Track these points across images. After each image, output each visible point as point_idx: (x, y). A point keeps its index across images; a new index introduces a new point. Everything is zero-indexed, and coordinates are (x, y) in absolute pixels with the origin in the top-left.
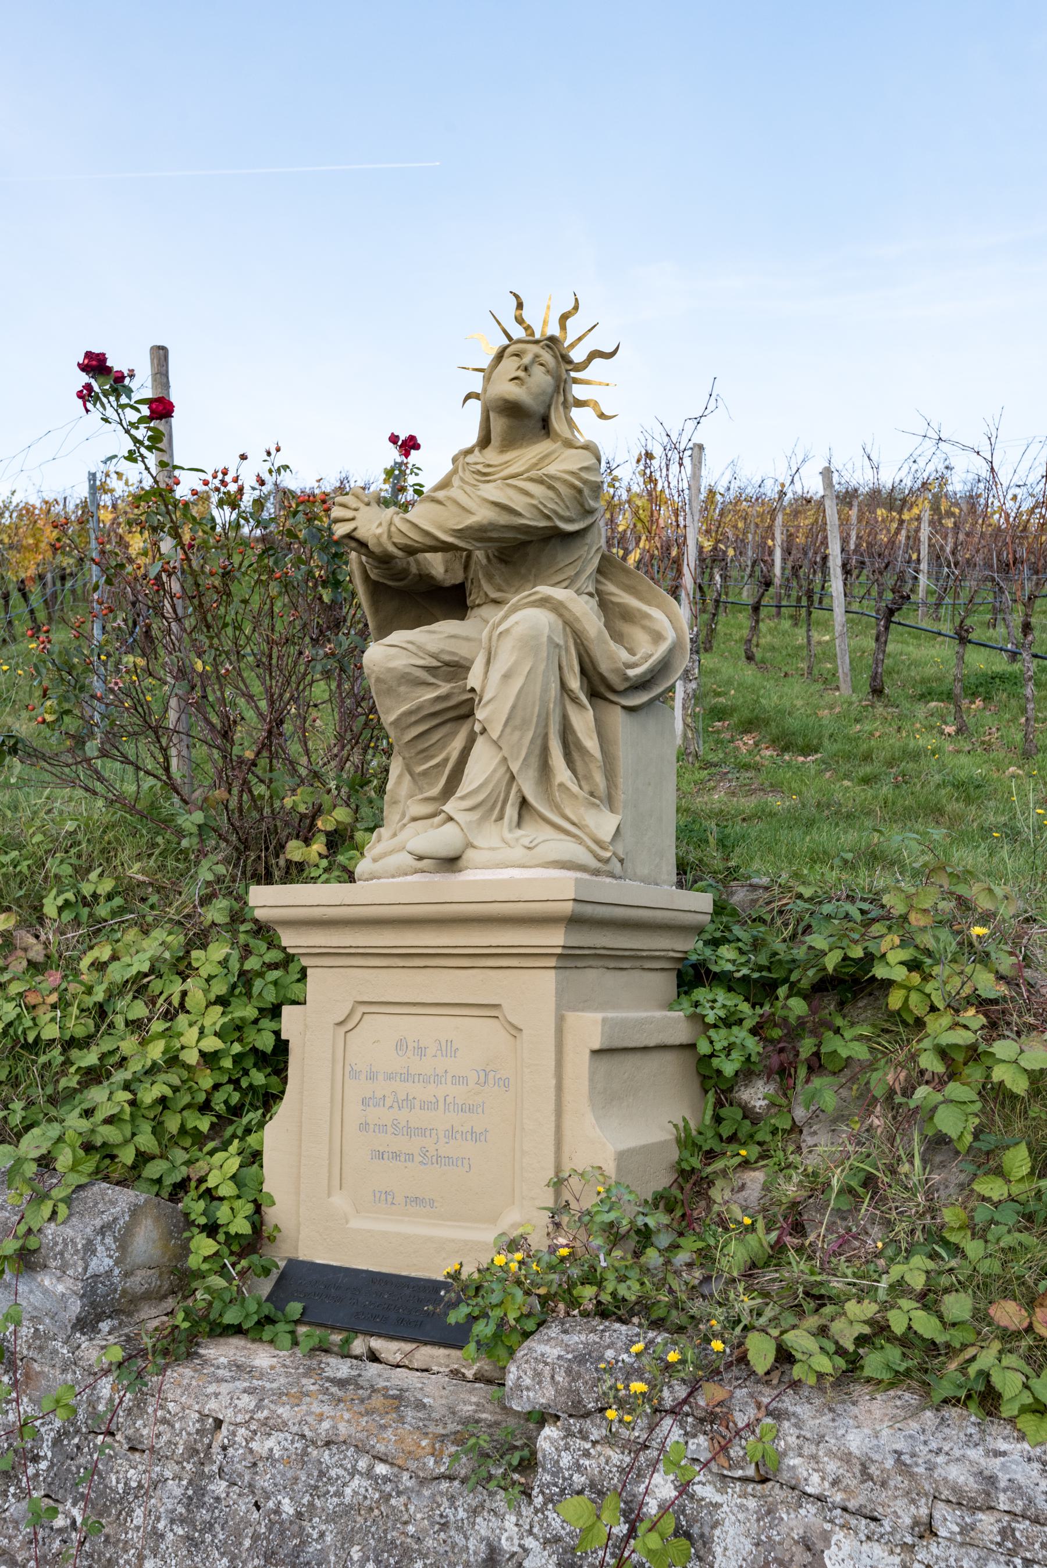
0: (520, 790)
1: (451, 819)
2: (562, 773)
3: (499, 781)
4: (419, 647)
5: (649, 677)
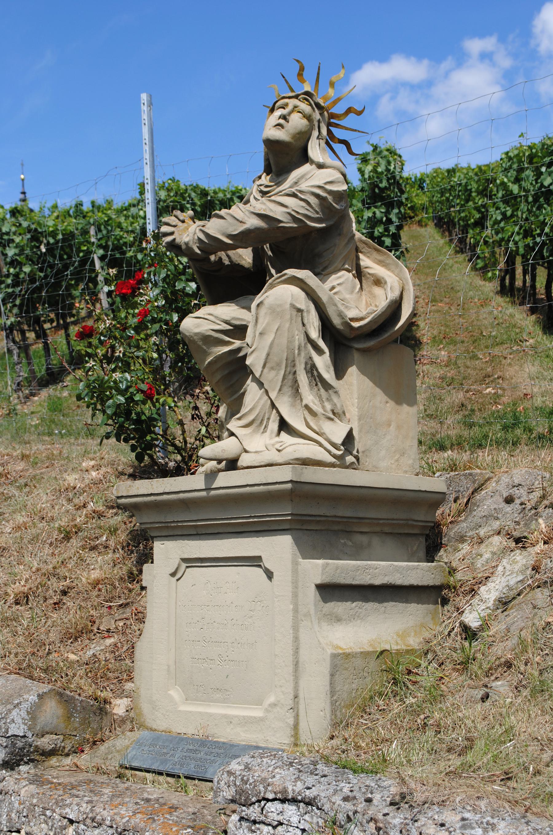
0: (278, 412)
1: (232, 434)
3: (264, 405)
4: (216, 317)
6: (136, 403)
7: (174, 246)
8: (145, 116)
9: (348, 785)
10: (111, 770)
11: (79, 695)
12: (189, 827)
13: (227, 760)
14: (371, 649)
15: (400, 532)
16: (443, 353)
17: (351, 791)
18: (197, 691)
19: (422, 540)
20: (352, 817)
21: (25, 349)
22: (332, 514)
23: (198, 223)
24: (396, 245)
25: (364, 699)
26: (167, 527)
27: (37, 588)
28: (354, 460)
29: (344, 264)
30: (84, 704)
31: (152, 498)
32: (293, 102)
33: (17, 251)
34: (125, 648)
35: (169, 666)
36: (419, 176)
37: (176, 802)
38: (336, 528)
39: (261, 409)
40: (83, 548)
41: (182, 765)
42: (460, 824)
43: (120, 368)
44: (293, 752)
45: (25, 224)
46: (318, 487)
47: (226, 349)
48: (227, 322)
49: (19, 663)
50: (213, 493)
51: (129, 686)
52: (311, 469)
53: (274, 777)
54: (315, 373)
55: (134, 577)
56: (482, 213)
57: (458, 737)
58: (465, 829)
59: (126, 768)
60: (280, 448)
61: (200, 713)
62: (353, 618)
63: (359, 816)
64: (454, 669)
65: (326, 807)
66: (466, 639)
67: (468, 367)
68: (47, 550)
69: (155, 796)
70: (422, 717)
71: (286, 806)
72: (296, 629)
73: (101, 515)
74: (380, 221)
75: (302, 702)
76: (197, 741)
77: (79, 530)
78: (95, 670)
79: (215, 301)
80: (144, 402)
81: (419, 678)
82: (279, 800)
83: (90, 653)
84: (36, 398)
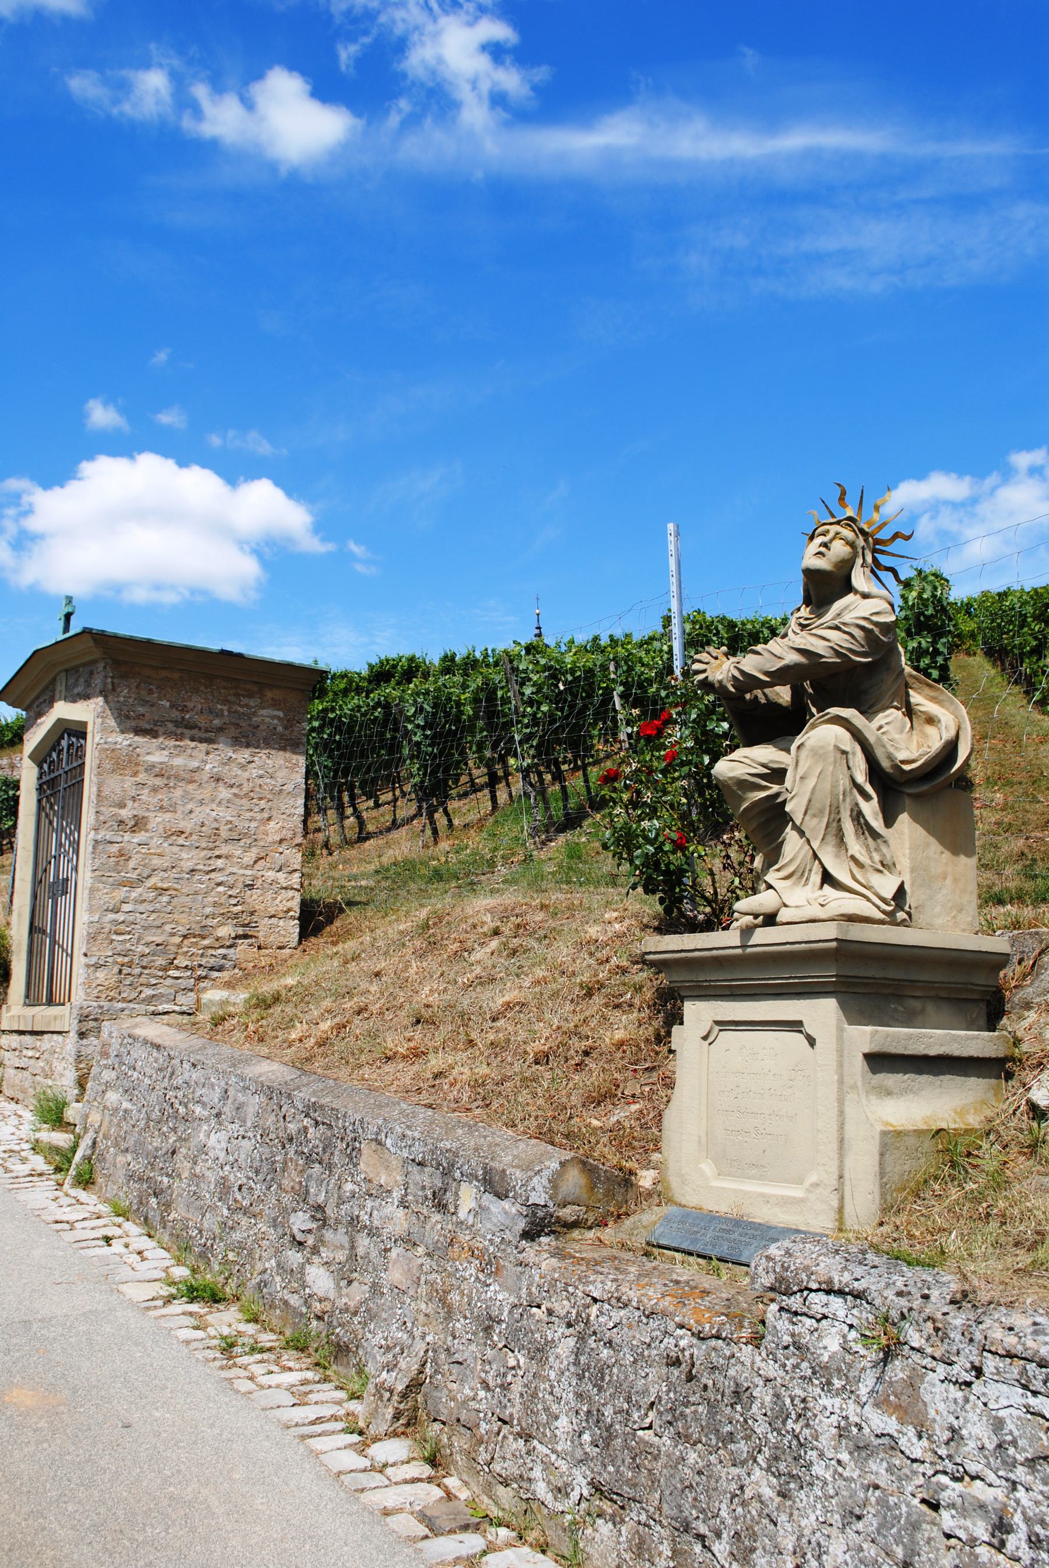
0: (821, 863)
1: (770, 887)
3: (805, 856)
4: (752, 760)
6: (666, 853)
7: (707, 685)
8: (672, 547)
9: (901, 1279)
10: (637, 1248)
11: (603, 1164)
12: (723, 1314)
13: (764, 1243)
14: (925, 1127)
15: (957, 996)
16: (998, 795)
17: (906, 1285)
18: (732, 1165)
19: (983, 1006)
20: (907, 1315)
21: (542, 793)
22: (881, 976)
23: (732, 659)
24: (944, 678)
25: (918, 1182)
26: (700, 987)
27: (558, 1048)
28: (905, 916)
29: (892, 702)
30: (608, 1175)
31: (683, 955)
32: (834, 529)
33: (534, 690)
34: (651, 1115)
35: (700, 1137)
36: (965, 600)
37: (707, 1286)
38: (886, 991)
39: (802, 859)
40: (606, 1005)
41: (714, 1246)
42: (1032, 1329)
43: (648, 814)
44: (838, 1238)
45: (543, 662)
46: (867, 946)
47: (763, 794)
49: (539, 1127)
50: (749, 950)
51: (655, 1156)
53: (818, 1265)
54: (862, 821)
55: (662, 1038)
56: (1039, 640)
57: (1026, 1230)
58: (1037, 1335)
59: (653, 1246)
61: (734, 1190)
62: (905, 1091)
63: (914, 1314)
64: (1020, 1152)
65: (878, 1302)
66: (1033, 1119)
67: (1027, 811)
68: (568, 1007)
69: (685, 1278)
70: (984, 1205)
71: (832, 1297)
72: (841, 1101)
73: (624, 971)
74: (926, 652)
75: (847, 1183)
76: (731, 1220)
77: (602, 986)
78: (619, 1138)
79: (750, 743)
80: (674, 852)
81: (980, 1162)
82: (824, 1290)
83: (613, 1119)
84: (553, 844)
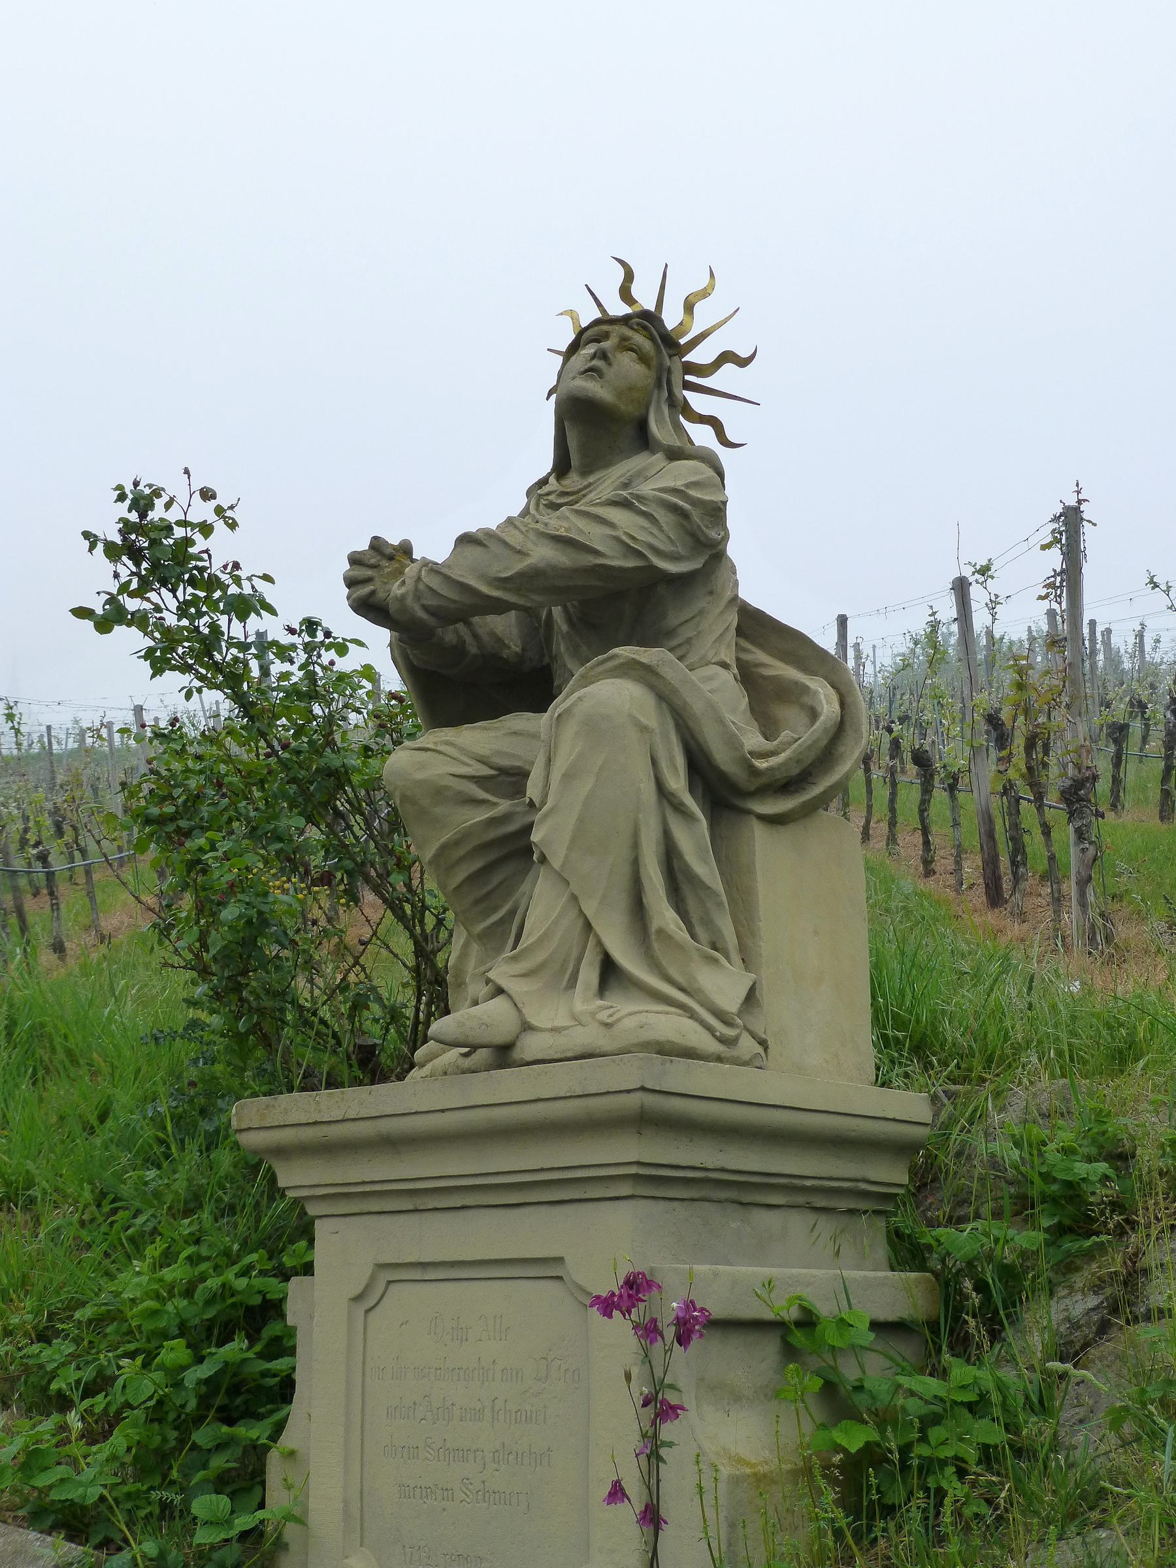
0: (599, 943)
2: (664, 915)
5: (795, 771)
48: (482, 761)
52: (681, 1063)
60: (609, 1021)
